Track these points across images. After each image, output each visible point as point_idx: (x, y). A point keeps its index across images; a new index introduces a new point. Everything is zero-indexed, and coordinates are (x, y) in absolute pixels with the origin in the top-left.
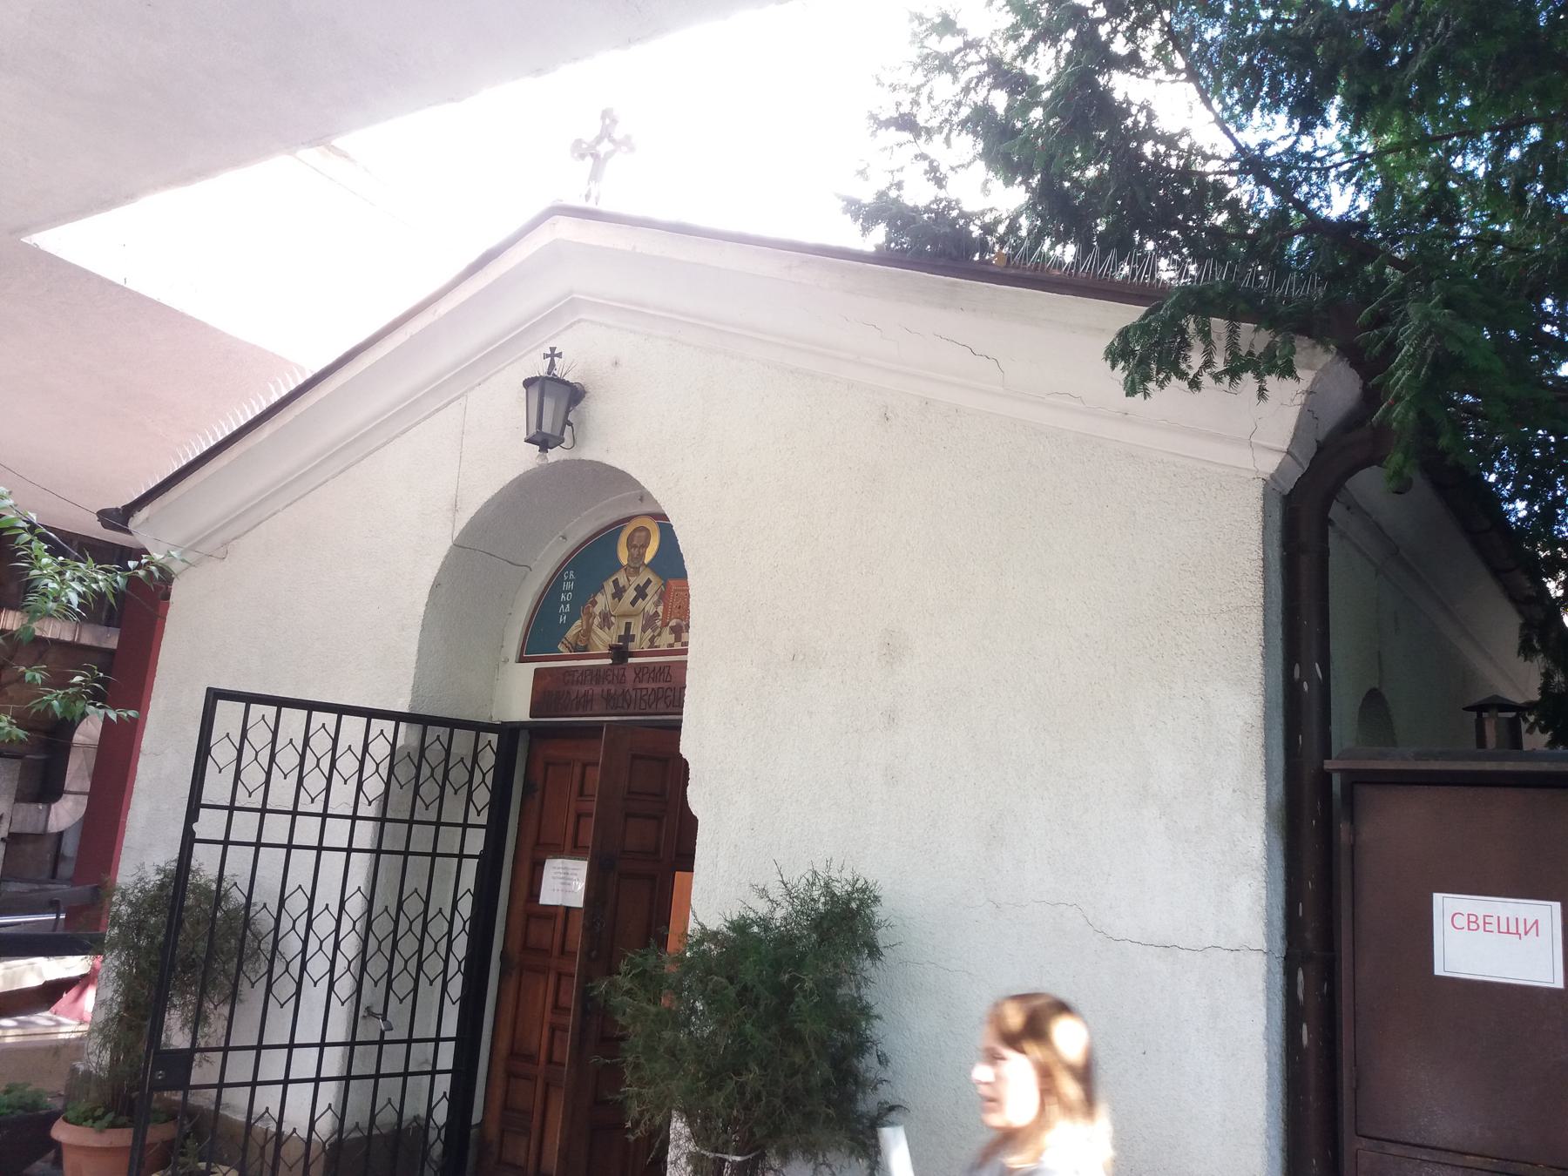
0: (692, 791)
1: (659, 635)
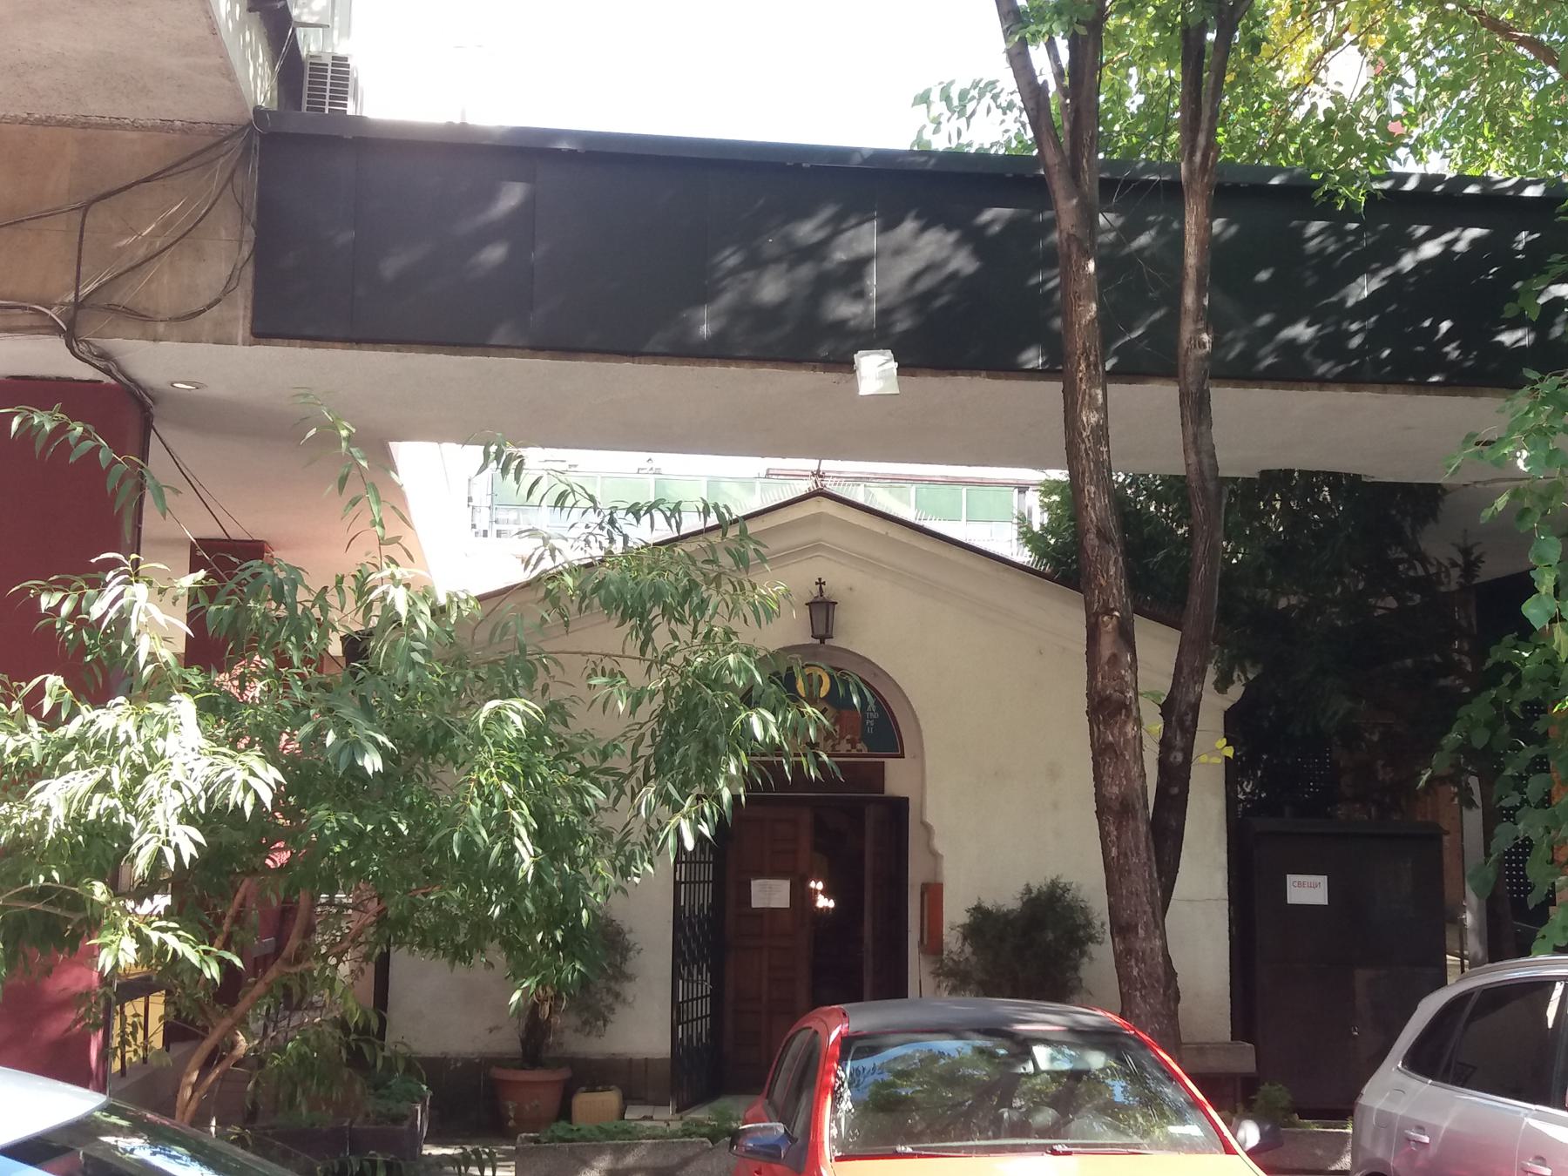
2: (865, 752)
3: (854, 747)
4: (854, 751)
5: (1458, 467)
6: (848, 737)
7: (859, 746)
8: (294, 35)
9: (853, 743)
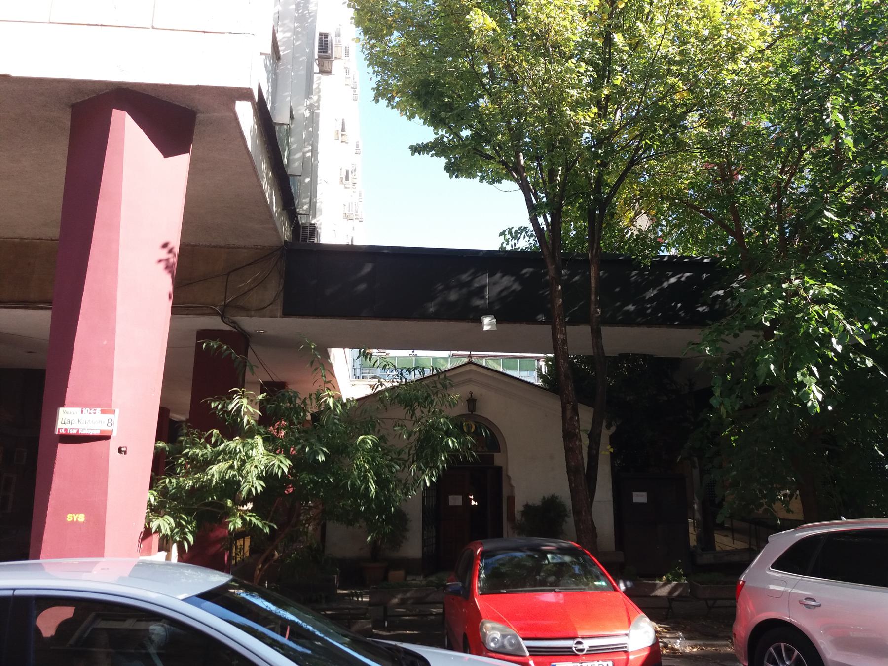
8: (297, 217)
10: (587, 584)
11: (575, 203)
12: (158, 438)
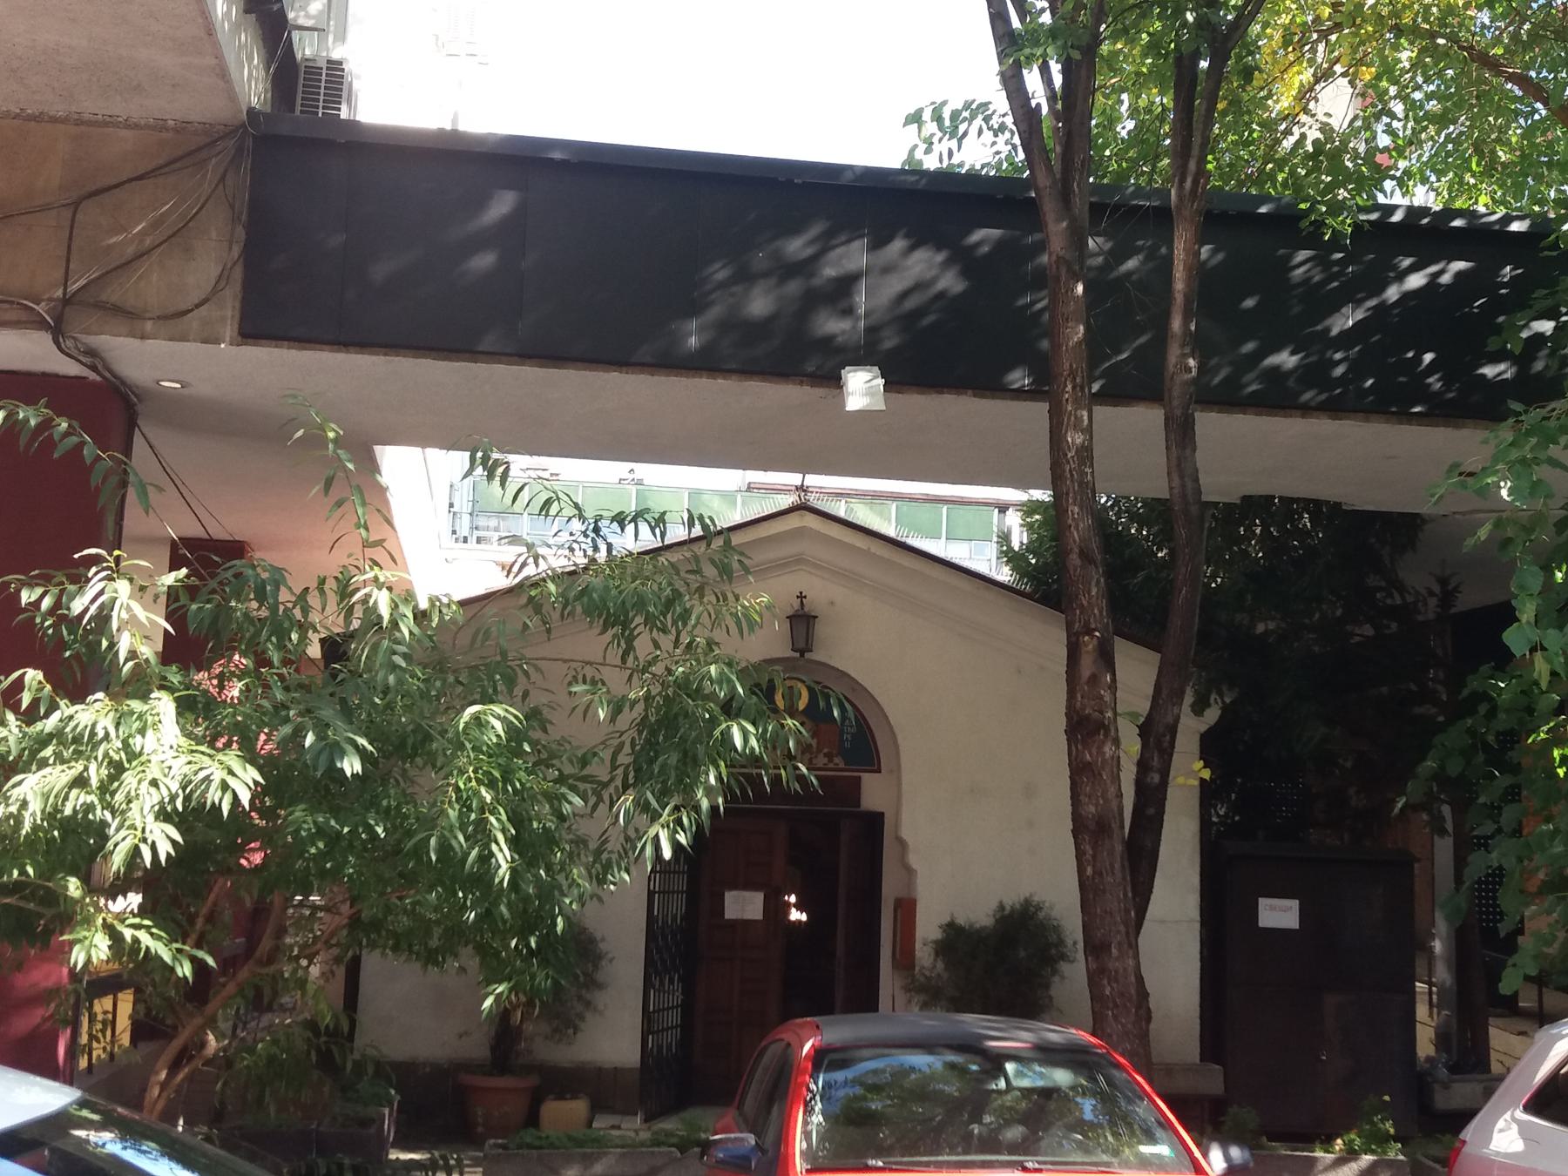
0: (676, 537)
1: (816, 757)
2: (842, 765)
3: (831, 761)
4: (831, 766)
5: (1441, 497)
6: (826, 750)
7: (836, 760)
9: (829, 756)
10: (1116, 1153)
11: (1139, 32)
12: (1281, 498)
